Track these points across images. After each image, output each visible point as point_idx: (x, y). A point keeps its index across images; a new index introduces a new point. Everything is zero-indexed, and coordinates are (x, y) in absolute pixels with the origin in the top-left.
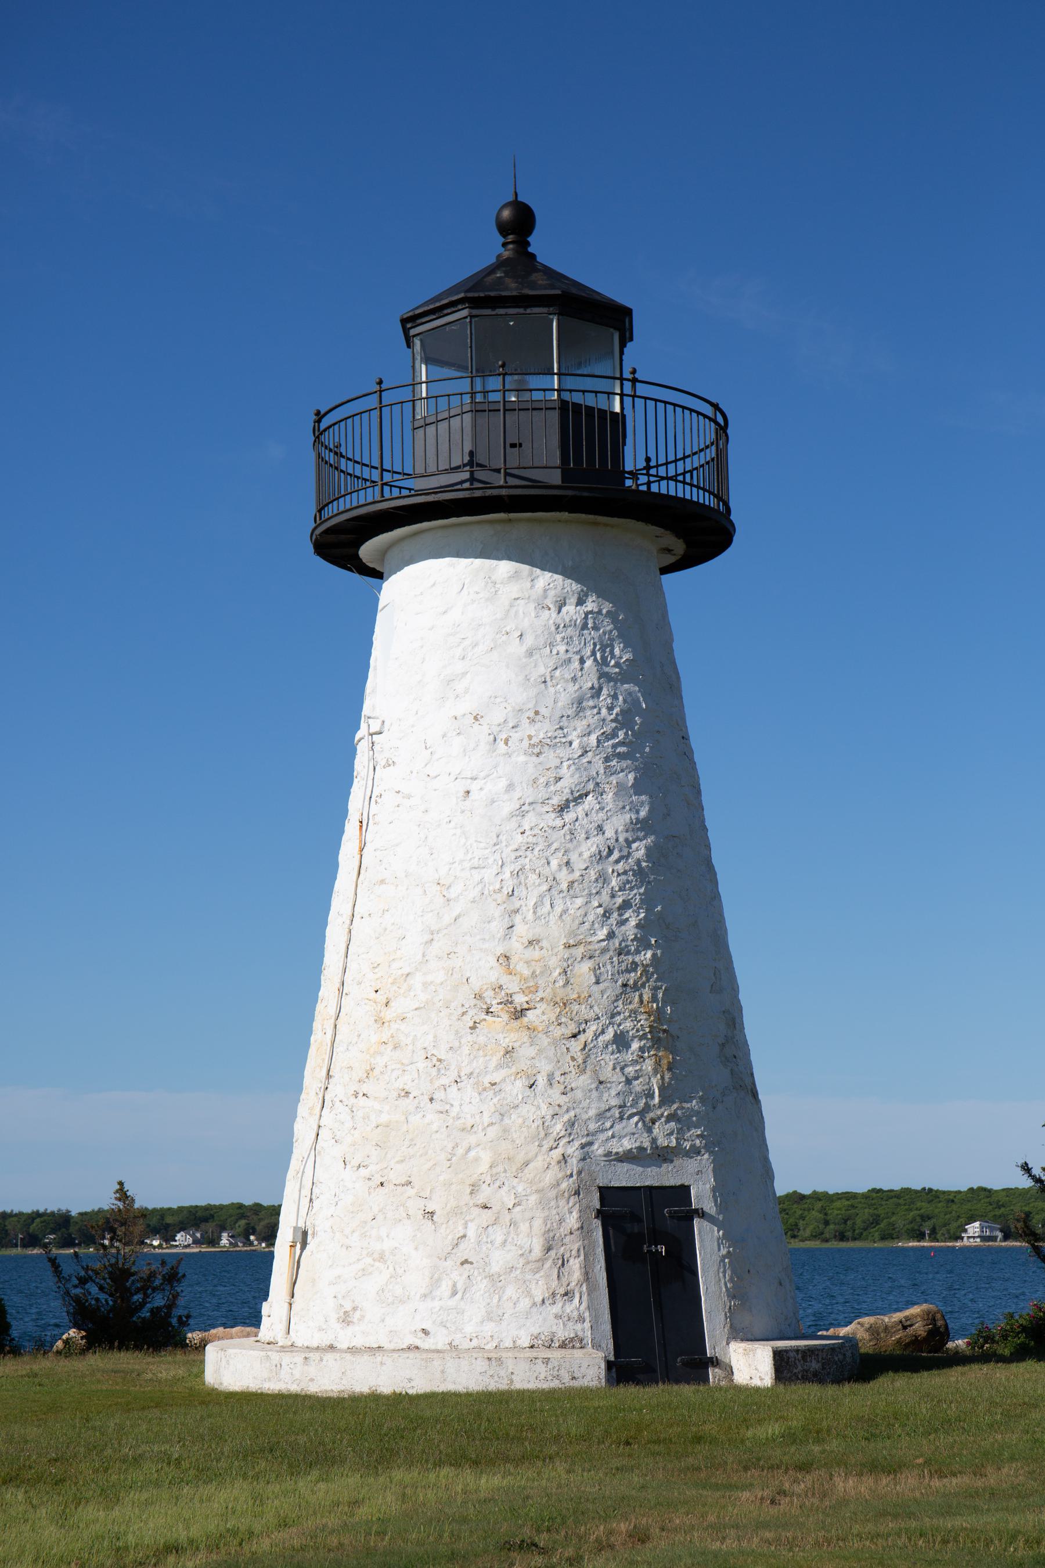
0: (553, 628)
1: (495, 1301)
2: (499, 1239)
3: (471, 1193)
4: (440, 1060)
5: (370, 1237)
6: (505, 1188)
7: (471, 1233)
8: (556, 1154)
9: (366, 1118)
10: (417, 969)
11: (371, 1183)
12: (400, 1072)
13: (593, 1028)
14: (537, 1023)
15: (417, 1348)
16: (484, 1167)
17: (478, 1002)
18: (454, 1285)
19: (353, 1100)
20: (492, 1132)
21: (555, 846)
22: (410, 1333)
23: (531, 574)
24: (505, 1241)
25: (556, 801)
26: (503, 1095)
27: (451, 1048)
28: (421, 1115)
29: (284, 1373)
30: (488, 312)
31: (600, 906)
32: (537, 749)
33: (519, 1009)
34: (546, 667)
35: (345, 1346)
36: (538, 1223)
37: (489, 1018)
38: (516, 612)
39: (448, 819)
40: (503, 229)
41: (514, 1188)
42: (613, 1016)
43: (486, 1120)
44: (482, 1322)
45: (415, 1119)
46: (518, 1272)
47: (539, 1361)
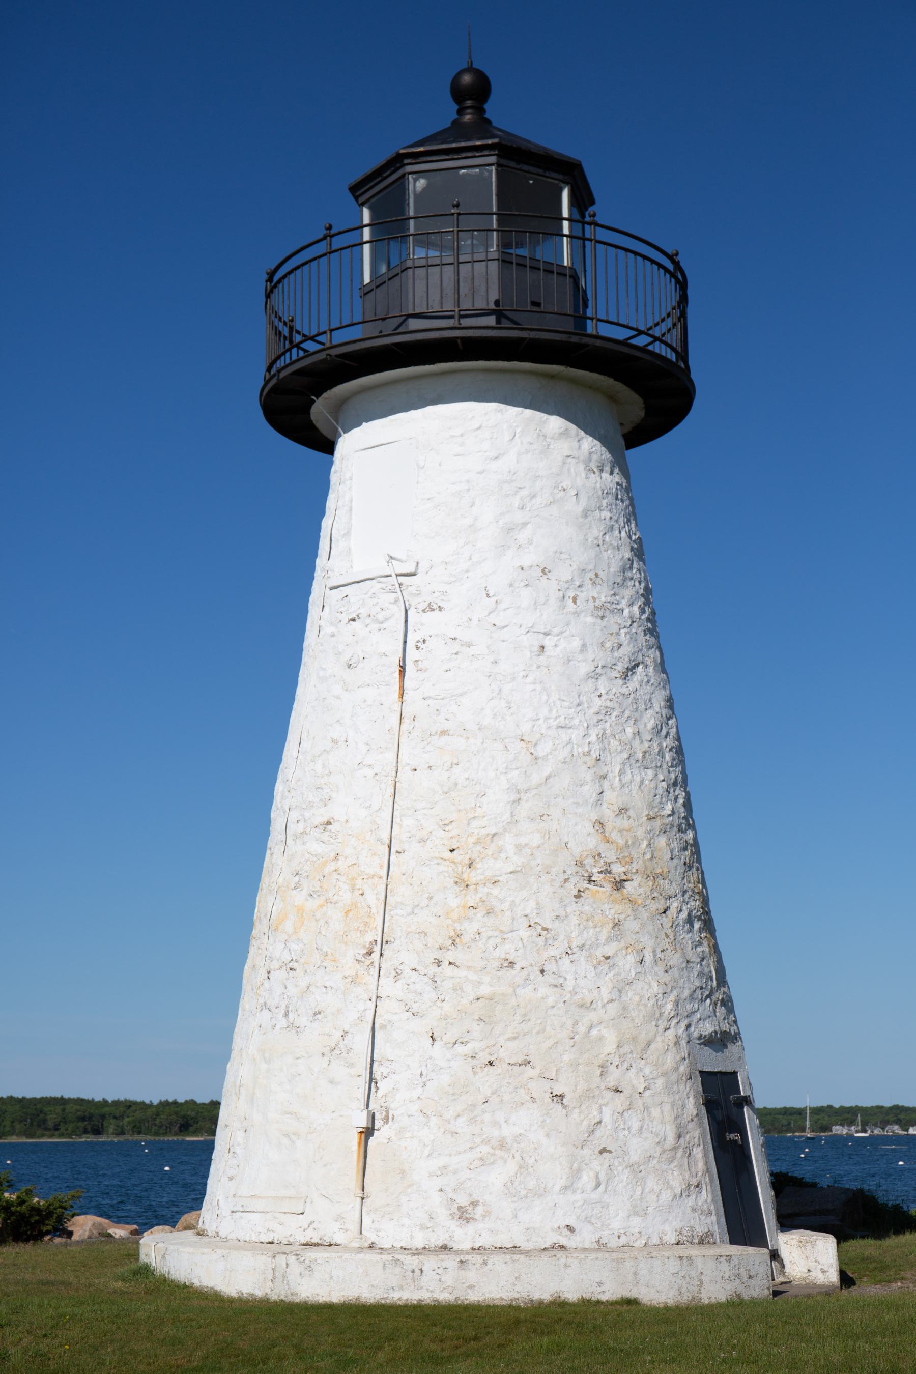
0: (600, 493)
1: (638, 1193)
2: (636, 1126)
3: (601, 1075)
4: (546, 929)
6: (633, 1070)
7: (607, 1118)
8: (671, 1033)
9: (458, 989)
10: (505, 830)
11: (475, 1062)
12: (499, 940)
13: (675, 905)
14: (635, 896)
16: (610, 1046)
17: (580, 869)
18: (597, 1177)
19: (433, 969)
20: (613, 1009)
21: (627, 713)
22: (552, 1230)
23: (577, 435)
25: (620, 667)
26: (617, 970)
27: (557, 917)
28: (531, 987)
29: (425, 1280)
32: (602, 611)
33: (618, 879)
35: (466, 1246)
36: (667, 1108)
37: (591, 887)
38: (569, 470)
39: (524, 673)
40: (459, 94)
41: (641, 1070)
43: (606, 996)
44: (628, 1217)
45: (526, 993)
46: (655, 1161)
47: (723, 1259)
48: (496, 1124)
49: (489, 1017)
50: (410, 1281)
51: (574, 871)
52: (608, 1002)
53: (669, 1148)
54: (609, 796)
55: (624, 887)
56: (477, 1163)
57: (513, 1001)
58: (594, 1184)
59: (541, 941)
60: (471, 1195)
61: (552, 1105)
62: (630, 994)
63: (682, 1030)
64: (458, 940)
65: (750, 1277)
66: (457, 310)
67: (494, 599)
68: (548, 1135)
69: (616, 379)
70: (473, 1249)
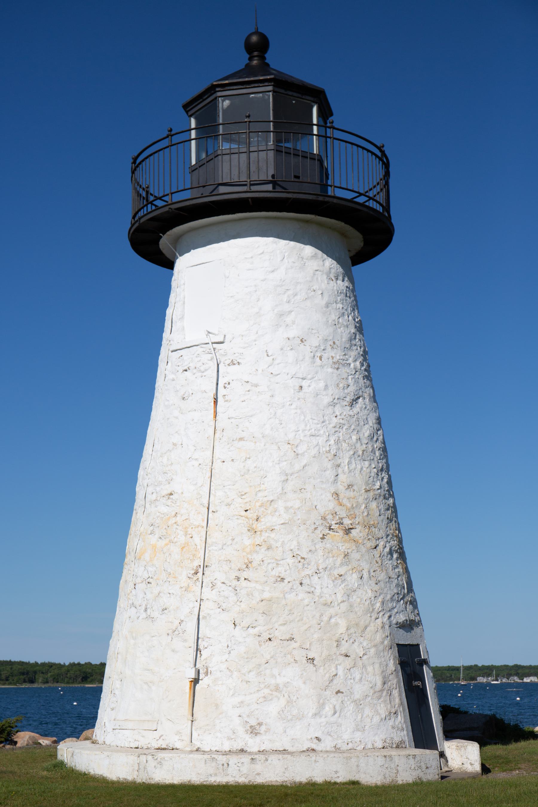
0: (336, 292)
1: (359, 717)
2: (358, 677)
3: (337, 646)
5: (265, 675)
6: (356, 644)
7: (340, 672)
8: (379, 621)
9: (250, 594)
10: (278, 498)
11: (260, 639)
12: (275, 565)
14: (358, 538)
15: (313, 750)
16: (342, 629)
17: (324, 522)
18: (334, 707)
19: (235, 583)
20: (344, 606)
21: (353, 427)
22: (307, 740)
23: (322, 257)
24: (361, 678)
25: (348, 399)
26: (346, 583)
27: (310, 551)
28: (294, 594)
30: (282, 91)
31: (375, 468)
32: (337, 365)
33: (347, 528)
34: (336, 316)
35: (255, 749)
36: (377, 666)
37: (331, 532)
38: (317, 279)
39: (290, 403)
40: (249, 48)
41: (361, 643)
42: (388, 536)
43: (340, 599)
44: (353, 732)
45: (291, 597)
46: (370, 698)
47: (411, 757)
48: (273, 676)
49: (269, 611)
50: (221, 771)
51: (320, 523)
52: (341, 602)
53: (378, 690)
54: (342, 477)
55: (351, 533)
56: (261, 700)
57: (284, 602)
58: (333, 712)
59: (300, 565)
60: (258, 719)
61: (307, 665)
62: (354, 597)
63: (386, 619)
64: (250, 565)
65: (427, 768)
66: (248, 180)
67: (272, 357)
68: (304, 683)
69: (346, 223)
70: (259, 751)
